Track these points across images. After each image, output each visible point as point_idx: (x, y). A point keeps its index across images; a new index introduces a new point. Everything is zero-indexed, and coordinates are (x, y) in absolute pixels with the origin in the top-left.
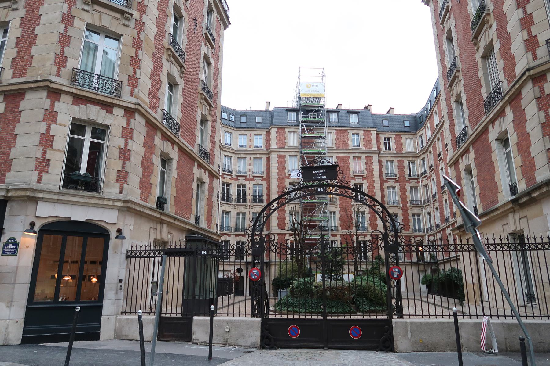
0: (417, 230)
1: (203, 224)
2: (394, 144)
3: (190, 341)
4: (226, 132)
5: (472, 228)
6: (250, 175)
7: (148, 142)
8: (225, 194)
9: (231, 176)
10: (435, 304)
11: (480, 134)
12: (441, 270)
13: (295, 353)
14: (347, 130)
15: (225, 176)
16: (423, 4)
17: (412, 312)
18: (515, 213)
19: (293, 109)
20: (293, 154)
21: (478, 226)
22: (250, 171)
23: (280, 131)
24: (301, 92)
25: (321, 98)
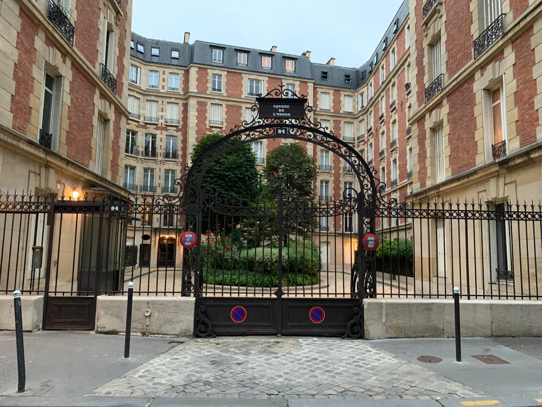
3: (93, 329)
6: (162, 123)
7: (25, 43)
18: (499, 178)
22: (162, 119)
23: (201, 71)
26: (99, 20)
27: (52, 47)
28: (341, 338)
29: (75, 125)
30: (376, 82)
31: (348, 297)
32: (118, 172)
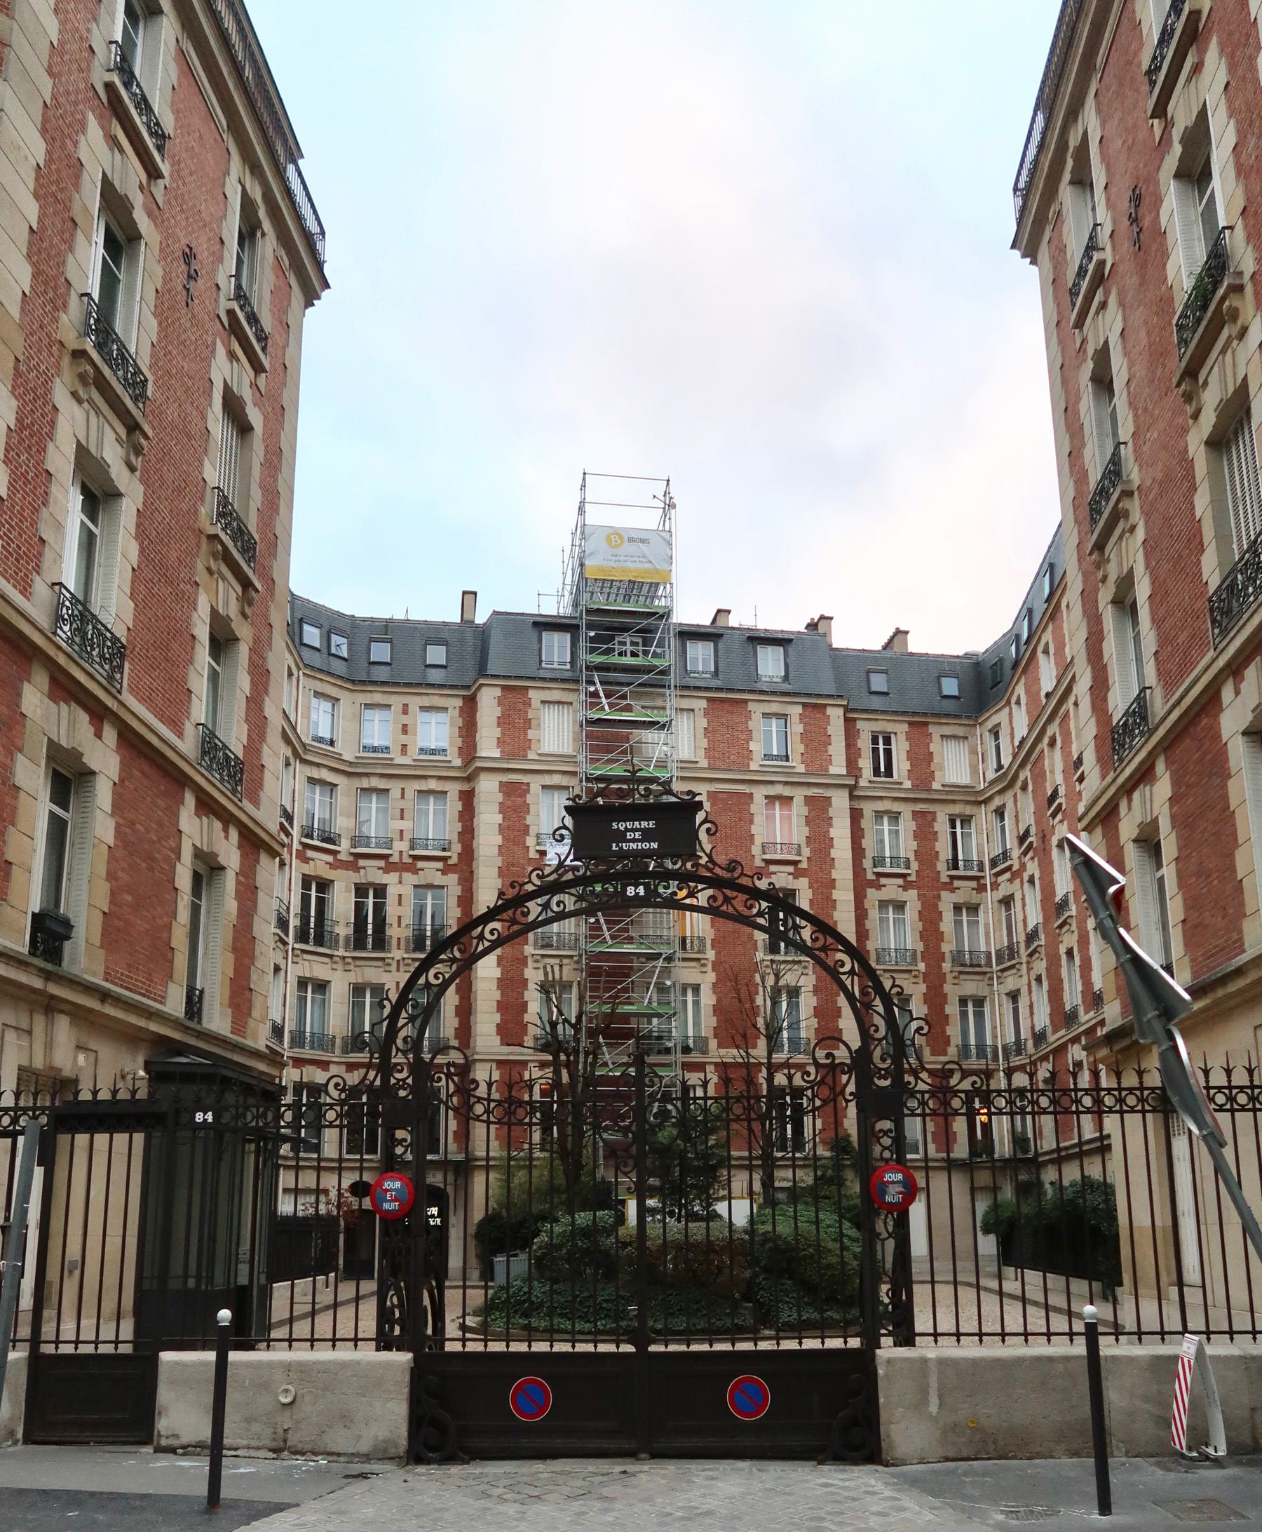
0: (974, 1051)
1: (217, 1020)
2: (904, 755)
3: (147, 1441)
4: (318, 694)
5: (1158, 1026)
8: (312, 920)
9: (334, 853)
10: (1024, 1300)
11: (1192, 714)
12: (1047, 1186)
13: (532, 1475)
14: (745, 702)
15: (310, 854)
16: (1017, 253)
17: (946, 1324)
19: (559, 621)
20: (556, 780)
21: (1183, 1016)
24: (587, 562)
25: (657, 585)
26: (195, 613)
27: (65, 702)
28: (815, 1463)
29: (128, 892)
30: (1032, 693)
31: (126, 1349)
32: (250, 1009)
